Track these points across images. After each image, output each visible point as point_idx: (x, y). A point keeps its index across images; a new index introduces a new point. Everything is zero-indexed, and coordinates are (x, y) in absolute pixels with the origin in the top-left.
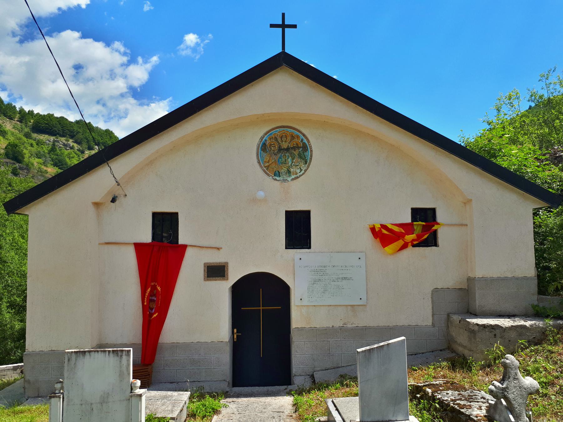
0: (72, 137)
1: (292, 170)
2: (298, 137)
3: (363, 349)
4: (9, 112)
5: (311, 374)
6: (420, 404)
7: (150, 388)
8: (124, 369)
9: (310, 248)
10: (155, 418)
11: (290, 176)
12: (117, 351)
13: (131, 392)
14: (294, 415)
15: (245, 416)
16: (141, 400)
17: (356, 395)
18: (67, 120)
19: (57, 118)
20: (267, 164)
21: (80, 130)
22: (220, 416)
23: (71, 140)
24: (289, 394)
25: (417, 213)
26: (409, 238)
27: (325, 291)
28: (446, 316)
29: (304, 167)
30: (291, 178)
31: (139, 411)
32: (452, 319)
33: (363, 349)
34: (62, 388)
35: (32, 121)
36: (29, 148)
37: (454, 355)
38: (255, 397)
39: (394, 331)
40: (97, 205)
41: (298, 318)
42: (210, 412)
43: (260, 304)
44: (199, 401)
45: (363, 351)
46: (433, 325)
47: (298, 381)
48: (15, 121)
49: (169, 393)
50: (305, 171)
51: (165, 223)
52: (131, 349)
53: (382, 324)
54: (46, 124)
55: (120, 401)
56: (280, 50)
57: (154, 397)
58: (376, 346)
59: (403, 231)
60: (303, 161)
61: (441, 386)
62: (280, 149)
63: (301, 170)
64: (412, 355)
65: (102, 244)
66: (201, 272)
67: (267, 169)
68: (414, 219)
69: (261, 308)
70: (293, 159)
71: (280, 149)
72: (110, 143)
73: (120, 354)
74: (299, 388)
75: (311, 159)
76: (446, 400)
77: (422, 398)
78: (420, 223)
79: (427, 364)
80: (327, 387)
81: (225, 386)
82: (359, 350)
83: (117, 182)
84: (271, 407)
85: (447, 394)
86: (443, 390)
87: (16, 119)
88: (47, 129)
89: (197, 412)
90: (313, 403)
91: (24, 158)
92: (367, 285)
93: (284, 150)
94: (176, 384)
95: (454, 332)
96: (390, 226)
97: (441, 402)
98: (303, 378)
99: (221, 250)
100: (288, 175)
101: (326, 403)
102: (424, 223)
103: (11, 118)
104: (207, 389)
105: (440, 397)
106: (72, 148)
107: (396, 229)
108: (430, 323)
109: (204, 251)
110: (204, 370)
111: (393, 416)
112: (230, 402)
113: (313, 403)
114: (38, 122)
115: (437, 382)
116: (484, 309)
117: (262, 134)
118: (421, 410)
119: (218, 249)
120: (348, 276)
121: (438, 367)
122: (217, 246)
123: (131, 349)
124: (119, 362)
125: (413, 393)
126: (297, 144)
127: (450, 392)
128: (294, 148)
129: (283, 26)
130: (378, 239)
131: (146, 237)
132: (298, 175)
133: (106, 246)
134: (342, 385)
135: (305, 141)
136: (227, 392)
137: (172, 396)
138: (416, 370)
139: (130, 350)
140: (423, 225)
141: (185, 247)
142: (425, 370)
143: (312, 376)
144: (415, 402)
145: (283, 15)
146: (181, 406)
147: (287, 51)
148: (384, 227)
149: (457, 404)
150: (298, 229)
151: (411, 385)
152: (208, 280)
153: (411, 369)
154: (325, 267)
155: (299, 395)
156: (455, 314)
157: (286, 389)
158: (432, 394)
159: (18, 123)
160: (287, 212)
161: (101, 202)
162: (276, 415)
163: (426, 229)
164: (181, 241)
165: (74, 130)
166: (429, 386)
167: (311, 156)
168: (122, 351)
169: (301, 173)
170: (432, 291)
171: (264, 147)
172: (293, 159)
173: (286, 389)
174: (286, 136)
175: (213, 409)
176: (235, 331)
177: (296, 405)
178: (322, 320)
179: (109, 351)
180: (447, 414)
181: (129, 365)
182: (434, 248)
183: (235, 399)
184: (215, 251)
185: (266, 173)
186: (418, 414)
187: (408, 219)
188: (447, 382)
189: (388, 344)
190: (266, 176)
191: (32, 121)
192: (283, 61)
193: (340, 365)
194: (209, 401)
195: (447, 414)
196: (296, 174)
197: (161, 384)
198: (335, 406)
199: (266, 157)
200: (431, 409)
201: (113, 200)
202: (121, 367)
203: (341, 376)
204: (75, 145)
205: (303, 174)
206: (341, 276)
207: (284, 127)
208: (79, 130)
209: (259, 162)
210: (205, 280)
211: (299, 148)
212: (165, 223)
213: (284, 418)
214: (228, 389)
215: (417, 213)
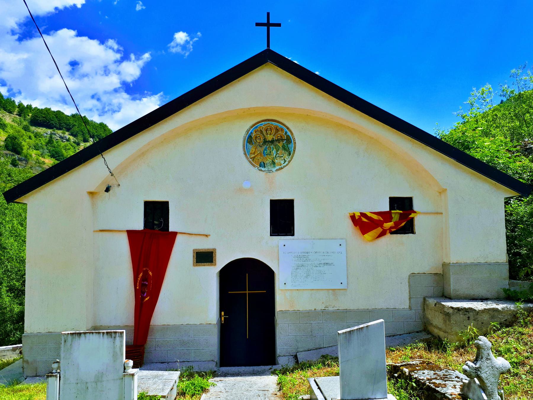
0: (68, 130)
1: (276, 161)
2: (282, 130)
3: (344, 331)
4: (8, 106)
5: (294, 354)
6: (398, 383)
8: (118, 350)
9: (293, 235)
11: (274, 167)
12: (111, 332)
13: (124, 372)
14: (278, 394)
16: (133, 379)
17: (337, 374)
18: (63, 113)
19: (54, 112)
20: (253, 156)
21: (76, 124)
22: (209, 394)
23: (67, 133)
24: (274, 373)
25: (395, 202)
26: (387, 225)
27: (307, 276)
28: (422, 300)
29: (287, 159)
31: (131, 390)
32: (427, 302)
34: (59, 368)
35: (30, 115)
36: (28, 140)
37: (430, 336)
38: (241, 376)
40: (91, 194)
41: (282, 301)
42: (199, 391)
43: (247, 288)
44: (188, 380)
45: (343, 333)
46: (410, 308)
47: (283, 361)
48: (15, 116)
49: (160, 372)
50: (289, 162)
51: (157, 212)
52: (124, 331)
53: (361, 307)
54: (44, 117)
55: (114, 380)
56: (265, 48)
58: (356, 328)
59: (382, 219)
63: (285, 161)
65: (97, 231)
66: (190, 258)
67: (253, 160)
68: (392, 207)
69: (247, 292)
70: (277, 151)
71: (265, 142)
73: (113, 335)
74: (283, 368)
75: (294, 151)
76: (422, 379)
77: (399, 377)
78: (398, 211)
79: (404, 345)
80: (310, 366)
81: (213, 366)
82: (340, 332)
84: (257, 386)
85: (423, 373)
86: (420, 370)
87: (15, 113)
88: (45, 122)
91: (22, 149)
94: (166, 364)
95: (430, 315)
96: (369, 215)
97: (418, 381)
98: (287, 358)
101: (309, 382)
102: (401, 212)
103: (10, 112)
104: (196, 369)
105: (416, 376)
106: (68, 140)
107: (375, 217)
108: (407, 306)
109: (193, 238)
111: (372, 394)
112: (218, 381)
113: (297, 382)
114: (36, 116)
115: (414, 362)
116: (458, 293)
117: (248, 127)
121: (415, 348)
122: (206, 233)
123: (124, 331)
124: (112, 343)
126: (281, 137)
127: (426, 371)
129: (268, 25)
131: (139, 225)
132: (282, 166)
133: (101, 233)
135: (289, 133)
136: (215, 371)
137: (162, 376)
138: (394, 351)
139: (123, 332)
140: (401, 213)
141: (175, 234)
143: (296, 357)
144: (393, 381)
145: (268, 14)
146: (172, 385)
147: (272, 48)
148: (363, 215)
150: (282, 217)
154: (307, 253)
155: (283, 374)
156: (431, 297)
157: (271, 369)
158: (409, 374)
159: (17, 116)
161: (96, 191)
162: (261, 393)
163: (402, 217)
164: (171, 229)
165: (70, 123)
167: (295, 148)
169: (285, 164)
170: (410, 276)
171: (249, 139)
172: (277, 151)
173: (271, 369)
175: (202, 387)
176: (223, 313)
179: (103, 333)
180: (423, 393)
183: (222, 378)
184: (204, 237)
186: (396, 392)
187: (386, 208)
189: (367, 326)
191: (30, 115)
193: (322, 346)
198: (317, 385)
200: (409, 388)
201: (107, 190)
202: (114, 348)
203: (323, 356)
204: (71, 138)
205: (287, 165)
206: (323, 262)
207: (269, 120)
209: (245, 154)
211: (283, 140)
212: (157, 212)
214: (215, 369)
215: (395, 202)
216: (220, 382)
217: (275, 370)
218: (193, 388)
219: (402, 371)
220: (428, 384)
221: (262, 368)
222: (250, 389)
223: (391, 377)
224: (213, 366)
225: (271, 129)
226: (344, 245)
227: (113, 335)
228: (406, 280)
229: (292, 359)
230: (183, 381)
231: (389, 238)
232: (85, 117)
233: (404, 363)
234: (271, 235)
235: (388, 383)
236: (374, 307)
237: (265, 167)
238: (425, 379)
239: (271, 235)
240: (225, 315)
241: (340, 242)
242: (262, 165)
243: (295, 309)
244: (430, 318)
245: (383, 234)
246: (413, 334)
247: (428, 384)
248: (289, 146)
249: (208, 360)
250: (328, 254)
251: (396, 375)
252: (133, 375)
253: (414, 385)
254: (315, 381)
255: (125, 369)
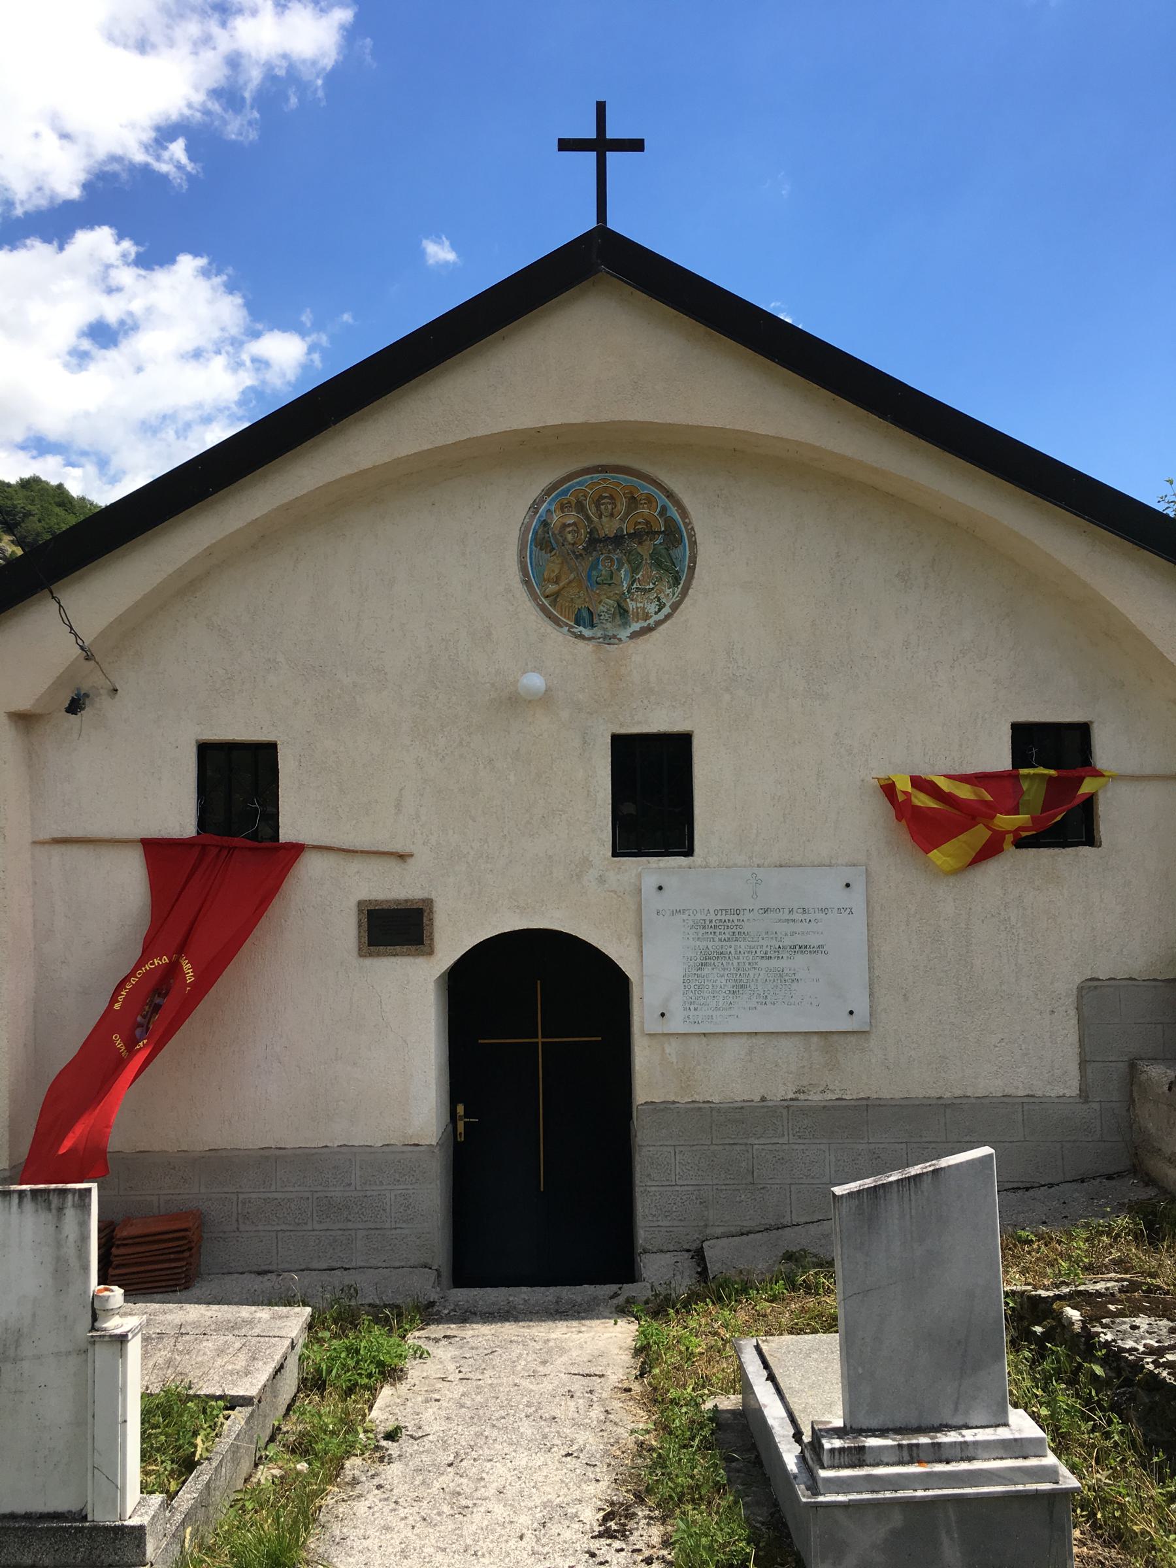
1: (631, 605)
2: (650, 499)
3: (853, 1186)
5: (694, 1246)
6: (1043, 1358)
7: (195, 1291)
8: (70, 1251)
9: (690, 852)
10: (190, 1398)
11: (625, 624)
12: (48, 1191)
13: (93, 1329)
14: (637, 1387)
15: (479, 1390)
16: (123, 1354)
17: (830, 1325)
20: (552, 588)
21: (34, 509)
22: (403, 1388)
24: (623, 1311)
25: (1030, 740)
26: (1006, 821)
27: (739, 988)
28: (1123, 1067)
29: (669, 595)
30: (630, 630)
31: (117, 1389)
32: (1144, 1077)
33: (853, 1186)
37: (1152, 1192)
38: (516, 1320)
39: (953, 1120)
40: (24, 720)
41: (653, 1075)
42: (370, 1376)
43: (537, 1029)
44: (336, 1336)
45: (851, 1194)
46: (1084, 1095)
47: (658, 1269)
49: (245, 1312)
50: (675, 607)
51: (238, 779)
52: (94, 1187)
53: (918, 1092)
55: (58, 1354)
56: (592, 223)
57: (195, 1324)
58: (894, 1177)
59: (989, 798)
60: (667, 578)
61: (1110, 1297)
62: (594, 541)
64: (1015, 1189)
65: (43, 843)
66: (346, 929)
67: (554, 603)
68: (1020, 757)
69: (540, 1040)
70: (635, 570)
71: (594, 541)
72: (58, 532)
73: (55, 1201)
74: (656, 1295)
75: (692, 569)
76: (1132, 1350)
77: (1048, 1336)
78: (1041, 770)
79: (1066, 1219)
80: (744, 1290)
81: (425, 1286)
82: (839, 1190)
83: (82, 648)
84: (565, 1358)
85: (1134, 1328)
86: (1120, 1314)
89: (329, 1372)
90: (699, 1345)
92: (871, 968)
93: (608, 545)
94: (273, 1277)
95: (1151, 1119)
96: (944, 784)
97: (1114, 1357)
98: (668, 1258)
99: (411, 861)
100: (618, 621)
101: (738, 1351)
102: (1052, 772)
104: (370, 1296)
105: (1109, 1337)
107: (964, 792)
108: (1071, 1088)
109: (355, 866)
110: (361, 1234)
111: (956, 1410)
112: (437, 1340)
113: (699, 1345)
115: (1100, 1286)
117: (535, 492)
118: (1047, 1379)
119: (402, 857)
120: (813, 941)
121: (1101, 1233)
122: (398, 847)
123: (94, 1187)
124: (51, 1229)
125: (1021, 1318)
126: (647, 523)
127: (1142, 1321)
128: (637, 536)
129: (601, 145)
130: (904, 821)
131: (178, 818)
132: (651, 621)
133: (57, 850)
134: (793, 1287)
136: (432, 1304)
137: (250, 1322)
138: (1030, 1242)
139: (89, 1190)
140: (1051, 777)
141: (296, 850)
142: (1059, 1242)
143: (699, 1255)
144: (1027, 1354)
145: (601, 108)
146: (278, 1357)
147: (615, 223)
148: (918, 783)
149: (1165, 1365)
150: (653, 794)
151: (1013, 1293)
152: (371, 955)
153: (1014, 1244)
154: (737, 912)
155: (655, 1315)
156: (1154, 1060)
157: (616, 1295)
158: (1084, 1328)
160: (616, 739)
161: (39, 711)
162: (578, 1385)
163: (1060, 790)
164: (286, 834)
165: (15, 506)
166: (1077, 1299)
167: (693, 559)
168: (65, 1191)
169: (661, 616)
170: (1080, 989)
171: (542, 540)
172: (635, 570)
173: (616, 1295)
174: (611, 497)
175: (380, 1364)
176: (460, 1109)
177: (644, 1352)
178: (727, 1079)
179: (21, 1193)
180: (1133, 1398)
181: (84, 1238)
182: (1085, 850)
183: (453, 1329)
184: (393, 865)
185: (549, 616)
186: (1039, 1392)
187: (1000, 758)
188: (1134, 1286)
189: (936, 1171)
190: (548, 627)
192: (601, 261)
193: (786, 1220)
194: (373, 1339)
195: (1133, 1398)
196: (647, 617)
197: (228, 1278)
198: (766, 1366)
199: (553, 567)
200: (1082, 1378)
202: (59, 1244)
203: (789, 1257)
205: (668, 617)
206: (787, 942)
207: (604, 469)
208: (29, 507)
209: (527, 583)
210: (362, 954)
211: (652, 534)
212: (238, 779)
213: (605, 1395)
214: (433, 1296)
215: (1030, 740)
216: (444, 1342)
217: (630, 1301)
218: (351, 1363)
219: (1059, 1316)
220: (1151, 1367)
221: (589, 1290)
222: (542, 1369)
223: (1020, 1338)
224: (425, 1286)
225: (611, 497)
226: (859, 887)
227: (55, 1201)
228: (1071, 1000)
229: (687, 1265)
230: (320, 1341)
231: (1016, 865)
232: (60, 486)
233: (1065, 1290)
234: (615, 854)
235: (1008, 1357)
236: (959, 1093)
237: (592, 626)
238: (1141, 1349)
239: (615, 854)
240: (466, 1115)
241: (848, 874)
242: (586, 618)
243: (697, 1098)
244: (1153, 1131)
245: (990, 851)
246: (1096, 1182)
247: (1151, 1367)
248: (675, 553)
249: (411, 1263)
250: (807, 917)
251: (1038, 1329)
252: (122, 1339)
253: (1098, 1370)
254: (758, 1348)
255: (95, 1318)
